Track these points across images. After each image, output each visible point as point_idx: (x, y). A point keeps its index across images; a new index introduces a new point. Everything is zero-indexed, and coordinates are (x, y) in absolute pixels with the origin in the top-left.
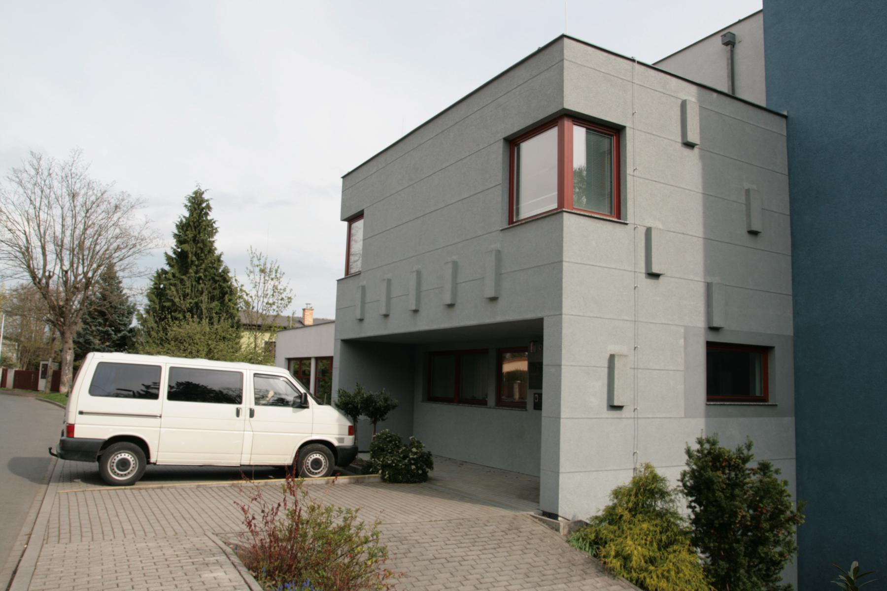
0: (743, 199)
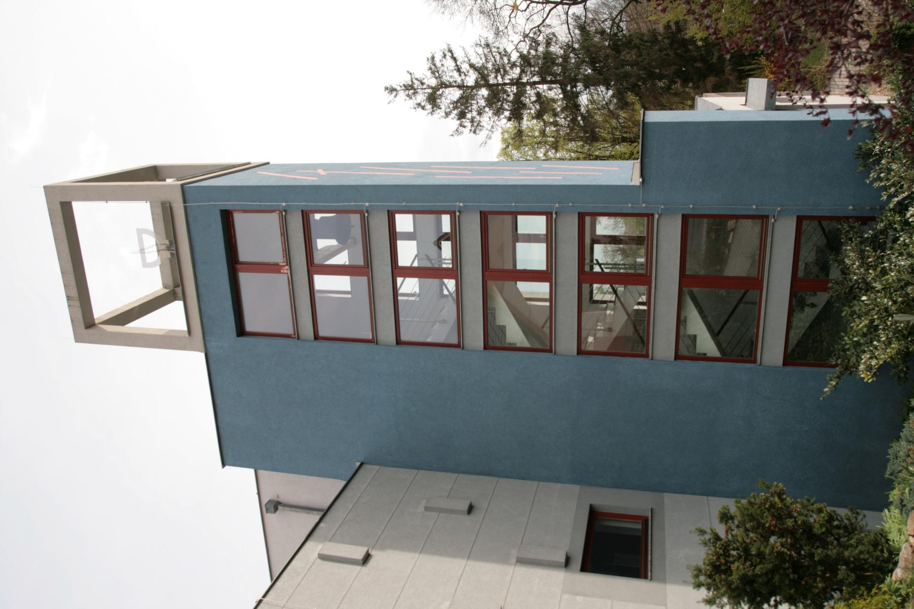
0: (435, 515)
